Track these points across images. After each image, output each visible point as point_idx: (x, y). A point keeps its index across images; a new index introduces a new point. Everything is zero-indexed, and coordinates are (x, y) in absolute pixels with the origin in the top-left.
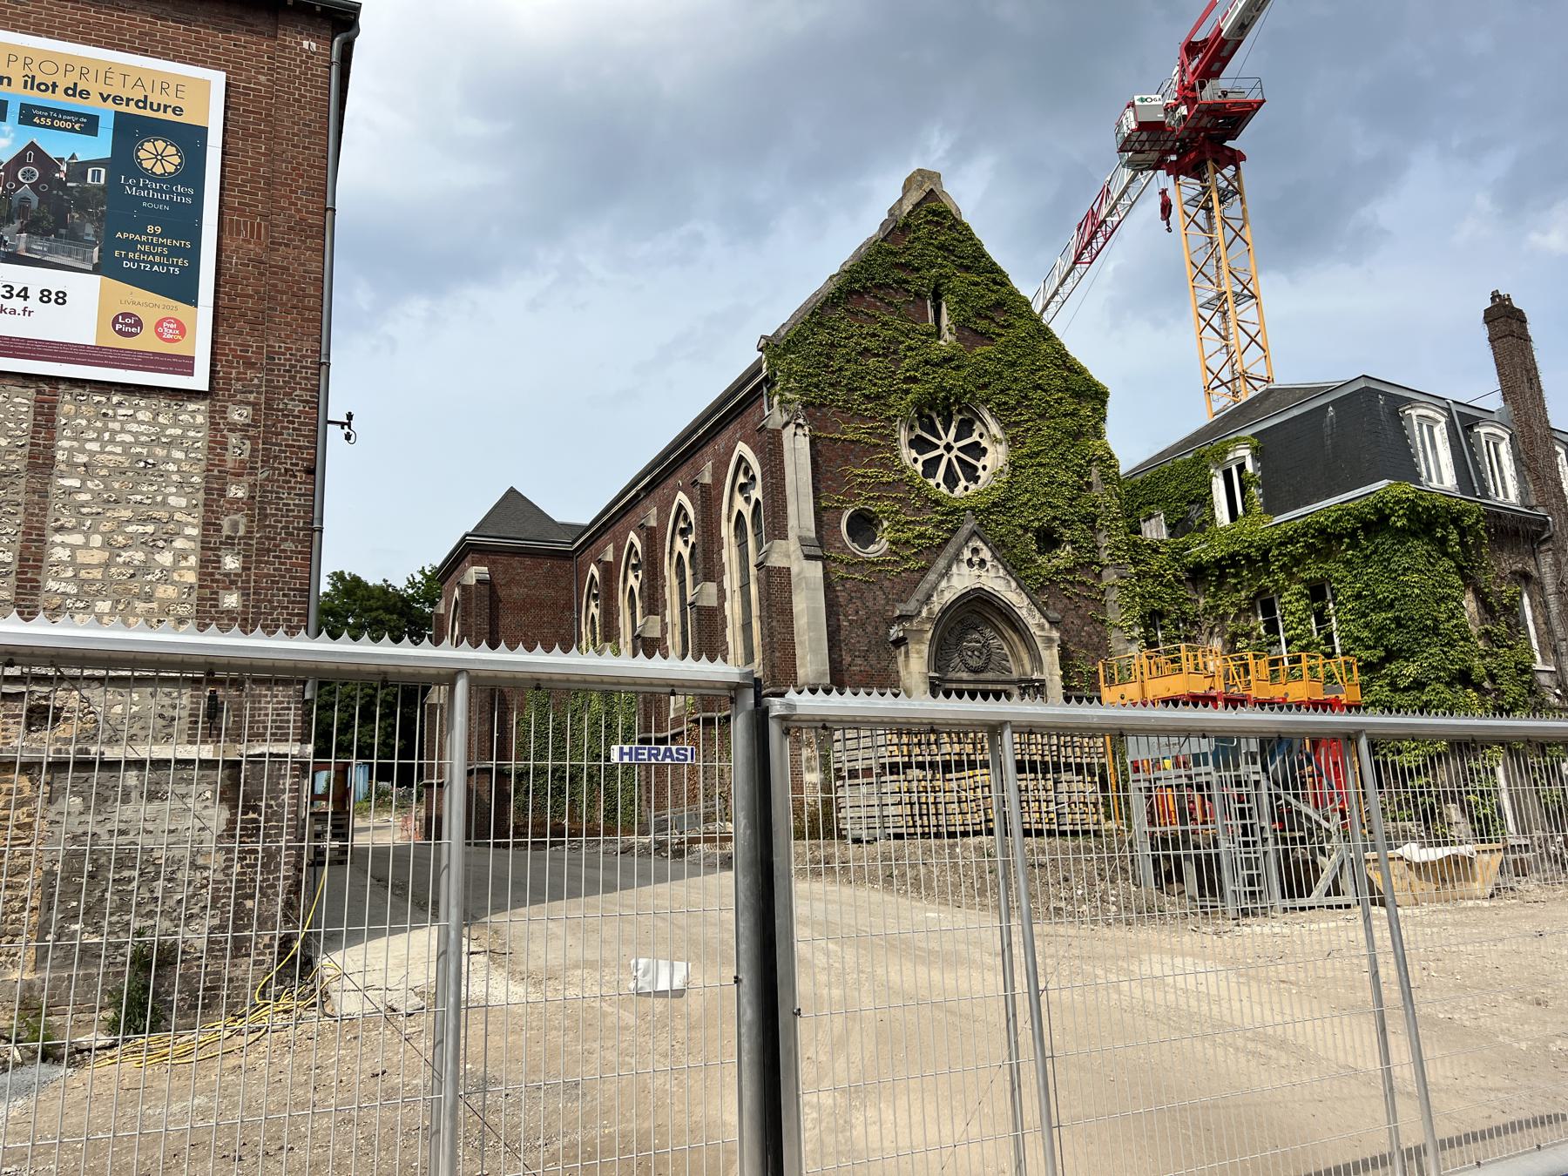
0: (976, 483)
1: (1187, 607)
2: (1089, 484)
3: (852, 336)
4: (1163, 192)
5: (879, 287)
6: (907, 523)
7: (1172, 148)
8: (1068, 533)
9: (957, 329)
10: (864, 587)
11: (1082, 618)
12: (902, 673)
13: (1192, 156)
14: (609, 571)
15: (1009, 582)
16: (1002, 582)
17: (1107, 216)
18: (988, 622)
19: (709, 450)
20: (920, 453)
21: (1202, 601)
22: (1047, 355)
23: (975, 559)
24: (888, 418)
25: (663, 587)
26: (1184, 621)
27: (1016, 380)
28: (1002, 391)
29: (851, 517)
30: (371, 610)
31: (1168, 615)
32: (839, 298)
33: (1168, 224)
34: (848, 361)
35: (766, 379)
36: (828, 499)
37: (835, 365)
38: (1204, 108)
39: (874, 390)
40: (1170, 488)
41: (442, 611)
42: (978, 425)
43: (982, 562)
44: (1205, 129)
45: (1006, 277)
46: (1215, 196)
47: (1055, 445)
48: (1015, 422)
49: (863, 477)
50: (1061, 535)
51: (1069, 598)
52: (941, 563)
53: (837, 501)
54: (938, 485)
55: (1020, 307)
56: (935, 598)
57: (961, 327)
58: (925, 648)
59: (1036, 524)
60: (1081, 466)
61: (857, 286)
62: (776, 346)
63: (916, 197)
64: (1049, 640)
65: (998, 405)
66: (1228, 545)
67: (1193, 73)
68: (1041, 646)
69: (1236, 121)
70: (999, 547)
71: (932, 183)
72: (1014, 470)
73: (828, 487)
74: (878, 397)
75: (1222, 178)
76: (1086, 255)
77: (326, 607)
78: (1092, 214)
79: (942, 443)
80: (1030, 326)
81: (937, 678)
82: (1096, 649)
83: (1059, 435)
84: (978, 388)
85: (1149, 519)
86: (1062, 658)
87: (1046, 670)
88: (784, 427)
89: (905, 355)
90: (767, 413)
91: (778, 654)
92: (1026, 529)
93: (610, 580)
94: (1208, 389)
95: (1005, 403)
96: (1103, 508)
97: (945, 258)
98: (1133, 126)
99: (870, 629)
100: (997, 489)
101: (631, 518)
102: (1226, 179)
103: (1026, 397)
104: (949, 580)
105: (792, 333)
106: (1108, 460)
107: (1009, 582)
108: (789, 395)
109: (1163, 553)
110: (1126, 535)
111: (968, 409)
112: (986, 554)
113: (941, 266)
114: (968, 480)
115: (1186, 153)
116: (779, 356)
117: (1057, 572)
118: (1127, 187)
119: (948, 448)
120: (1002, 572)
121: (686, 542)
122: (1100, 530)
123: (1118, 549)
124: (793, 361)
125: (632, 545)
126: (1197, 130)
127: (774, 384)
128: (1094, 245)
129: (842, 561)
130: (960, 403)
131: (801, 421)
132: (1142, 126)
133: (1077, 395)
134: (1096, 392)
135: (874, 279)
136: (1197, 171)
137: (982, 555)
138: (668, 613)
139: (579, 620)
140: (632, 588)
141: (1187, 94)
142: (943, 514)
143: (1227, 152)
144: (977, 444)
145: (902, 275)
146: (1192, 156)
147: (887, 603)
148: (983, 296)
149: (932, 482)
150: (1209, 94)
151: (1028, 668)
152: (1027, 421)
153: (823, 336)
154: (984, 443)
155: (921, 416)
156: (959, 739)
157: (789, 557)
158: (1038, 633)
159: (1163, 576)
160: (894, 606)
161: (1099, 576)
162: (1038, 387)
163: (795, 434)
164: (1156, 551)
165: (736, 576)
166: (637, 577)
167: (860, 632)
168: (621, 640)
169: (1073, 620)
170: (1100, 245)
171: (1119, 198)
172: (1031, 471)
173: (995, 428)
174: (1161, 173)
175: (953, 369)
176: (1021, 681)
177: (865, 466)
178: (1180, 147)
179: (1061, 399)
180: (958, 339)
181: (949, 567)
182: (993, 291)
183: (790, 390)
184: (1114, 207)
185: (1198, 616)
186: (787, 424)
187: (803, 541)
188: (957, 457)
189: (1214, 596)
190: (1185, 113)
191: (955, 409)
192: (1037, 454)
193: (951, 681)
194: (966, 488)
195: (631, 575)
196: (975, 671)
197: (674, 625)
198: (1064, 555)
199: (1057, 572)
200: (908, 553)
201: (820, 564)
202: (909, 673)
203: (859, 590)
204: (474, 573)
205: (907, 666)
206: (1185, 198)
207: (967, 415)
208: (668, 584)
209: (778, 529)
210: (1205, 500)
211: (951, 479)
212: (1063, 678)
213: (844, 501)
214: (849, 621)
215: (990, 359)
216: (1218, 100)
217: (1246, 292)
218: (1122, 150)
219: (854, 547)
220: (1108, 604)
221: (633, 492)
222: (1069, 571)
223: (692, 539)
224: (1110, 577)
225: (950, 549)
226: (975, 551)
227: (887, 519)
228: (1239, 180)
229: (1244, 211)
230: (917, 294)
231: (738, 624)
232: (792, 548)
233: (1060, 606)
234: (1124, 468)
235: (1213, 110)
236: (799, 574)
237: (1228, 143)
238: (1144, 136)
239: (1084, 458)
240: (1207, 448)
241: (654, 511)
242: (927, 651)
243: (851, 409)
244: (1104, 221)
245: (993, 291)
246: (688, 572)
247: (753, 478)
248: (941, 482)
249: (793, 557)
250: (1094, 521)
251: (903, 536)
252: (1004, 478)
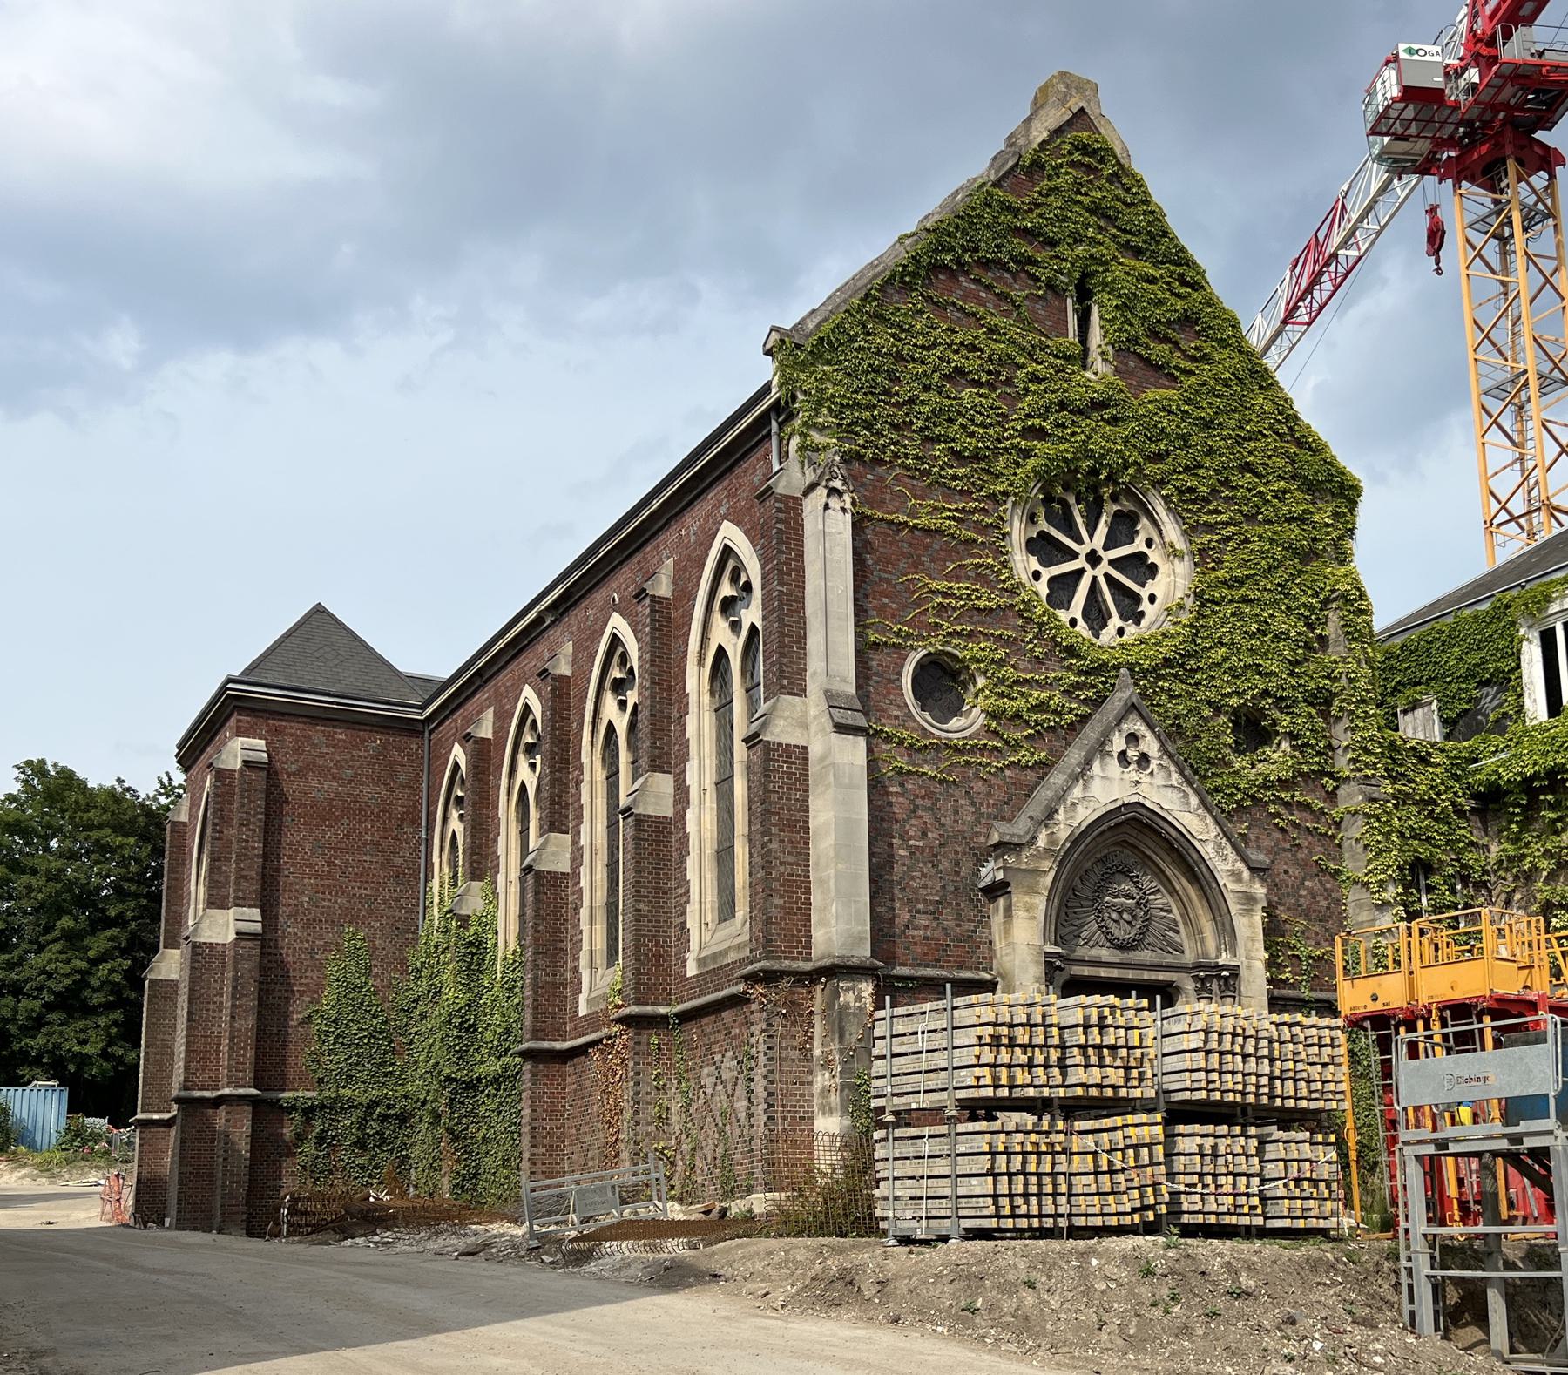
0: (1138, 623)
1: (1470, 857)
2: (1323, 640)
3: (935, 345)
4: (1433, 211)
5: (986, 264)
6: (1017, 682)
7: (1451, 137)
8: (1286, 720)
9: (1117, 352)
10: (938, 789)
11: (1303, 865)
12: (999, 945)
13: (1484, 149)
14: (484, 756)
15: (1186, 796)
16: (1176, 796)
17: (1340, 247)
18: (1147, 862)
19: (669, 537)
20: (1047, 563)
21: (1494, 848)
22: (1263, 415)
23: (1132, 753)
24: (992, 497)
25: (578, 783)
26: (1465, 880)
27: (1210, 452)
28: (1187, 469)
29: (921, 667)
30: (90, 827)
31: (1440, 869)
32: (915, 275)
33: (1438, 263)
34: (927, 388)
35: (776, 407)
36: (881, 629)
37: (903, 392)
38: (1507, 70)
39: (971, 443)
40: (1450, 658)
41: (184, 818)
42: (1144, 524)
43: (1144, 759)
44: (1505, 106)
45: (1202, 274)
46: (1516, 217)
47: (1271, 569)
48: (1206, 524)
49: (945, 595)
50: (1274, 723)
51: (1283, 830)
52: (1074, 756)
53: (898, 634)
54: (1073, 622)
55: (1226, 332)
56: (1060, 816)
57: (1124, 350)
58: (1040, 902)
59: (1234, 701)
60: (1311, 608)
61: (947, 258)
62: (799, 347)
63: (1054, 117)
64: (1249, 899)
65: (1181, 492)
66: (1545, 754)
67: (1491, 17)
68: (1234, 908)
69: (1555, 98)
70: (1172, 733)
71: (1084, 98)
72: (1203, 605)
73: (881, 609)
74: (976, 457)
75: (1523, 191)
76: (1303, 310)
77: (10, 819)
78: (1315, 246)
79: (1083, 550)
80: (1237, 361)
81: (1059, 956)
82: (1324, 920)
83: (1278, 552)
84: (1148, 459)
85: (1413, 709)
86: (1267, 932)
87: (1241, 951)
88: (806, 493)
89: (1026, 389)
90: (776, 467)
91: (778, 901)
92: (1218, 710)
93: (487, 772)
94: (1490, 526)
95: (1192, 490)
96: (1344, 682)
97: (1101, 229)
98: (1395, 92)
99: (945, 865)
100: (1172, 637)
101: (529, 662)
102: (1534, 191)
103: (1226, 483)
104: (1085, 786)
105: (827, 327)
106: (1355, 602)
107: (1186, 796)
108: (817, 438)
109: (1437, 765)
110: (1379, 729)
111: (1130, 494)
112: (1150, 745)
113: (1094, 242)
114: (1123, 617)
115: (1473, 145)
116: (803, 365)
117: (1266, 786)
118: (1374, 201)
119: (1094, 559)
120: (1175, 778)
121: (622, 704)
122: (1340, 719)
123: (1367, 751)
124: (826, 377)
125: (527, 709)
126: (1494, 107)
127: (791, 416)
128: (1316, 294)
129: (901, 742)
130: (1116, 483)
131: (837, 484)
132: (1410, 94)
133: (1311, 487)
134: (1342, 486)
135: (976, 250)
136: (1489, 176)
137: (1143, 747)
138: (585, 829)
139: (429, 843)
140: (523, 786)
141: (1482, 49)
142: (1080, 673)
143: (1537, 149)
144: (1141, 556)
145: (1028, 250)
146: (1484, 149)
147: (977, 822)
148: (1161, 302)
149: (1064, 616)
150: (1516, 49)
151: (1211, 945)
152: (1227, 524)
153: (883, 339)
154: (1154, 556)
155: (1048, 500)
156: (1101, 1058)
157: (806, 727)
158: (1231, 886)
159: (1435, 803)
160: (989, 826)
161: (1332, 796)
162: (1247, 468)
163: (827, 507)
164: (1424, 760)
165: (710, 763)
166: (533, 766)
167: (927, 869)
168: (501, 878)
169: (1287, 869)
170: (1326, 295)
171: (1361, 219)
172: (1229, 610)
173: (1173, 532)
174: (1430, 180)
175: (1108, 422)
176: (1199, 967)
177: (948, 577)
178: (1466, 134)
179: (1284, 492)
180: (1117, 372)
181: (1087, 763)
182: (1177, 295)
183: (821, 429)
184: (1352, 233)
185: (1485, 872)
186: (812, 487)
187: (833, 701)
188: (1107, 576)
189: (1516, 840)
190: (1476, 79)
191: (1107, 491)
192: (1241, 582)
193: (1082, 962)
194: (1121, 632)
195: (523, 763)
196: (1122, 947)
197: (594, 851)
198: (1279, 757)
199: (1266, 786)
200: (1017, 735)
201: (861, 742)
202: (1010, 944)
203: (928, 795)
204: (237, 750)
205: (1007, 931)
206: (1470, 218)
207: (1127, 505)
208: (586, 777)
209: (789, 679)
210: (1507, 680)
211: (1095, 614)
212: (1271, 964)
213: (909, 636)
214: (909, 848)
215: (1170, 412)
216: (1529, 58)
217: (1556, 374)
218: (1374, 132)
219: (924, 718)
220: (1346, 844)
221: (532, 615)
222: (1284, 784)
223: (632, 697)
224: (1351, 798)
225: (1091, 733)
226: (1133, 738)
227: (984, 673)
228: (1553, 196)
229: (1559, 245)
230: (1050, 286)
231: (710, 848)
232: (812, 712)
233: (1267, 843)
234: (1381, 621)
235: (1526, 77)
236: (823, 758)
237: (1540, 135)
238: (1410, 113)
239: (1316, 594)
240: (1515, 592)
241: (569, 648)
242: (1042, 906)
243: (928, 473)
244: (1334, 256)
245: (1177, 295)
246: (624, 757)
247: (748, 587)
248: (1079, 617)
249: (813, 728)
250: (1328, 703)
251: (1012, 706)
252: (1185, 618)
